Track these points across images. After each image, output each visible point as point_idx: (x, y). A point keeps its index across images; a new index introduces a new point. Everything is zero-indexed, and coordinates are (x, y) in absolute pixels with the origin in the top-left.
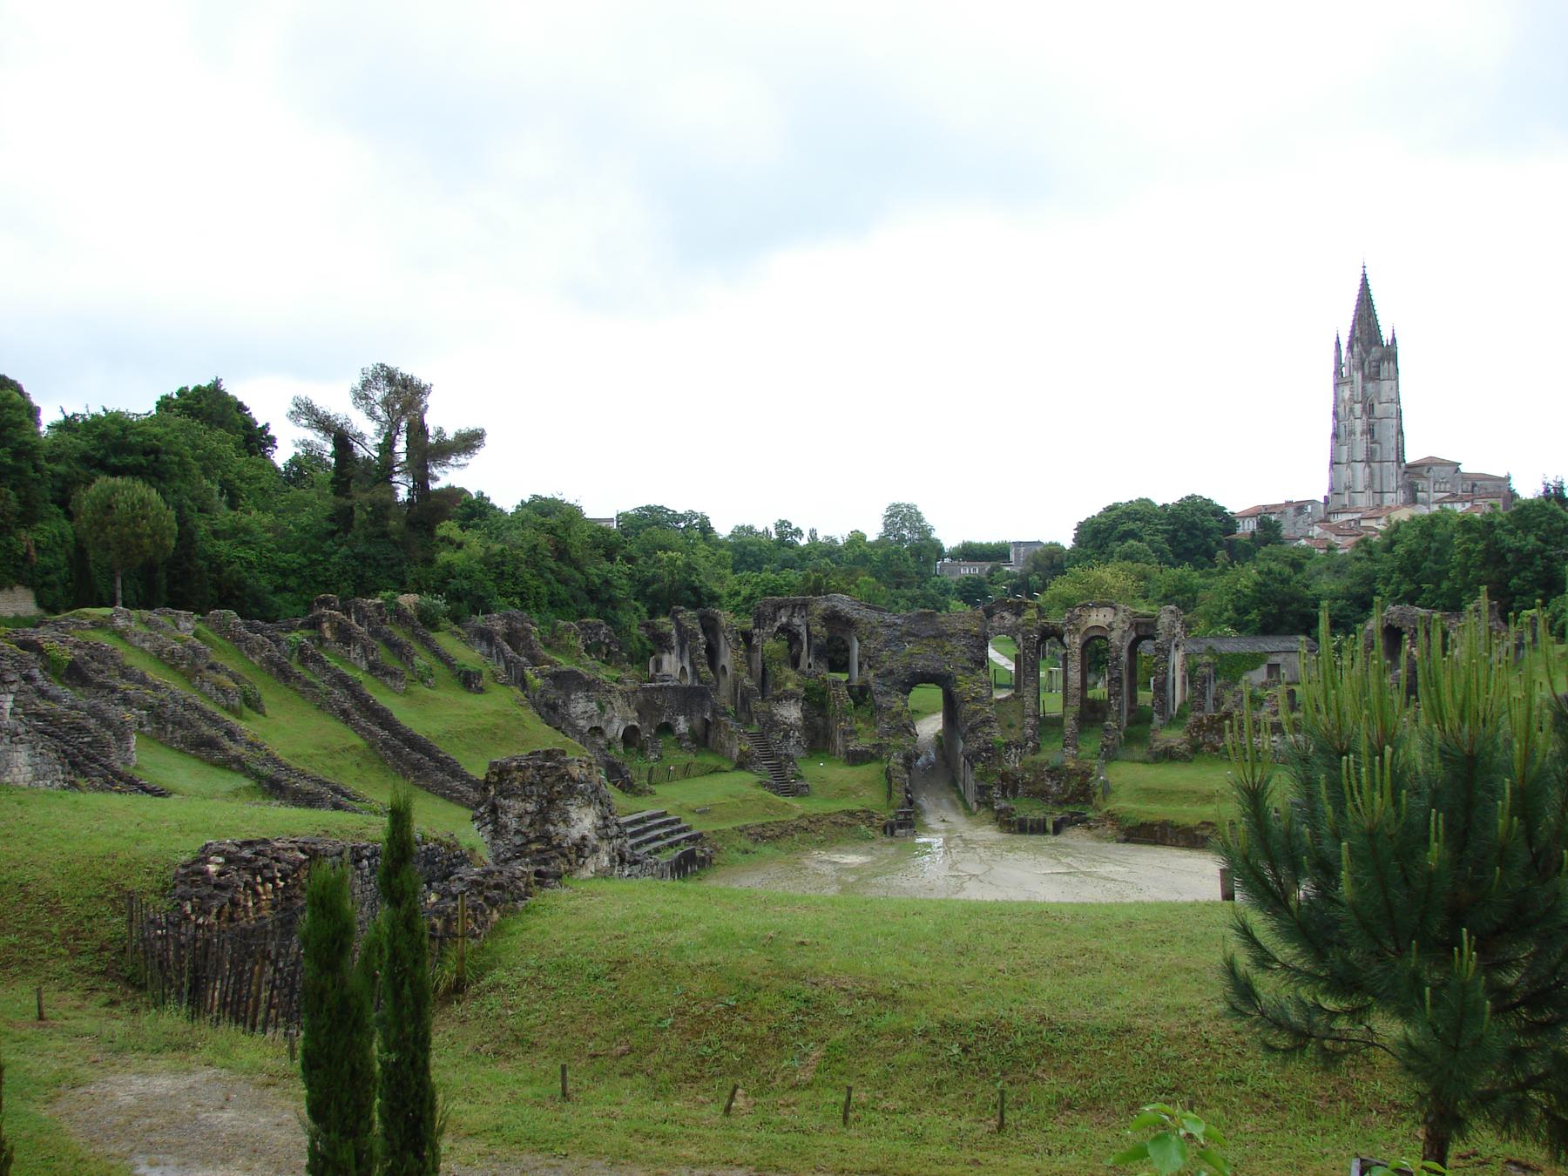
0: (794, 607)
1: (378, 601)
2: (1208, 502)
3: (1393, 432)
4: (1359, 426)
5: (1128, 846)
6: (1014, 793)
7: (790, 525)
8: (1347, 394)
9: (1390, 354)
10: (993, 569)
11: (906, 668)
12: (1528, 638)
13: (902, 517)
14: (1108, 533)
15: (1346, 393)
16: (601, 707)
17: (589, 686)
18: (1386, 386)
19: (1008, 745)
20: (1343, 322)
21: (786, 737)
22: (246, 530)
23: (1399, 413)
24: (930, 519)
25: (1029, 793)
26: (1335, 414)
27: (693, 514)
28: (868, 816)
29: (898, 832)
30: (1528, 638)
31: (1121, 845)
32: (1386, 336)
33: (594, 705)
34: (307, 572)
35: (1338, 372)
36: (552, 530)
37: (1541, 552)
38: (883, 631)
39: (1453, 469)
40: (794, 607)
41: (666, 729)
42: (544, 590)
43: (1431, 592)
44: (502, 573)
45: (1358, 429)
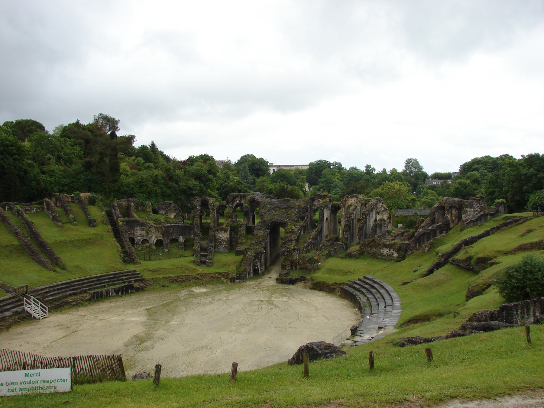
0: (241, 197)
1: (73, 195)
5: (313, 291)
6: (296, 268)
7: (370, 166)
10: (444, 182)
11: (270, 220)
13: (412, 164)
16: (147, 232)
17: (142, 225)
19: (294, 250)
21: (220, 244)
22: (53, 171)
24: (421, 164)
25: (301, 268)
28: (227, 275)
29: (236, 281)
31: (310, 290)
33: (144, 232)
34: (71, 185)
36: (168, 170)
37: (536, 175)
38: (268, 206)
40: (241, 197)
41: (176, 240)
42: (159, 191)
43: (499, 191)
44: (142, 185)
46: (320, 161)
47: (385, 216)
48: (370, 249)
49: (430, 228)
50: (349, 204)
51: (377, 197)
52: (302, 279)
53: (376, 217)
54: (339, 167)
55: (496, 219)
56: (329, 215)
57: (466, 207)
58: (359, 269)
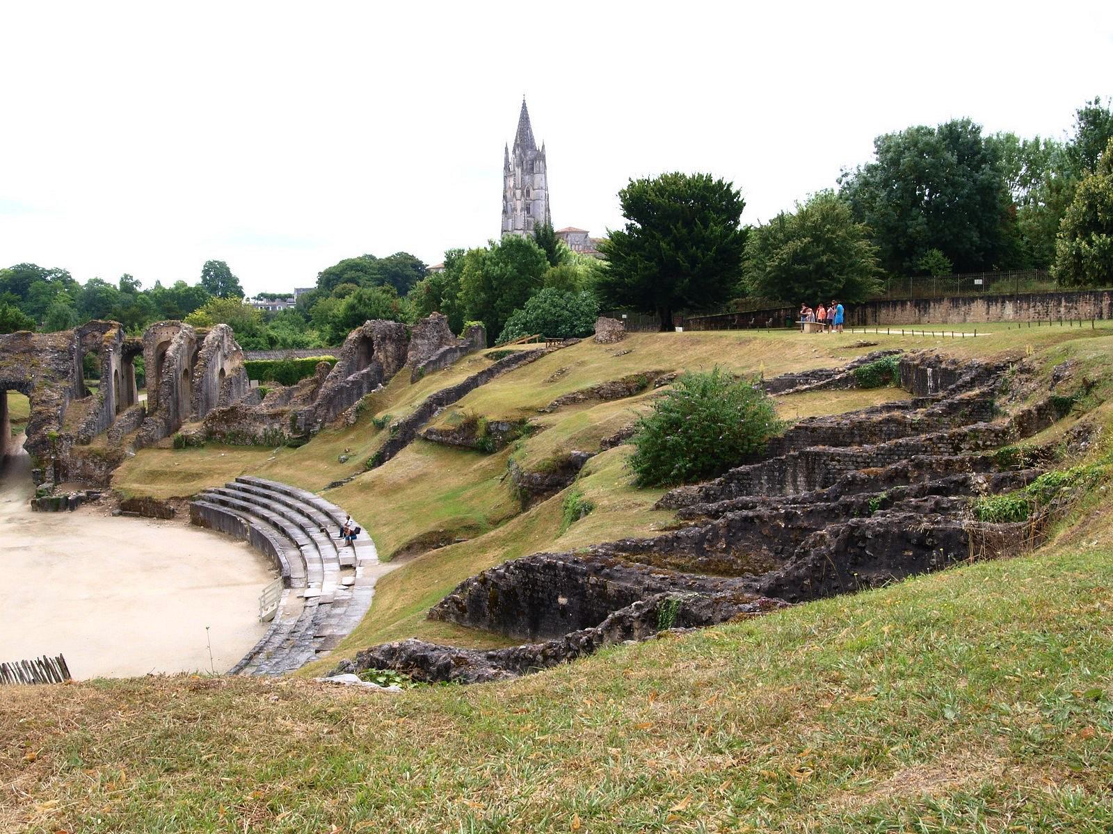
2: (412, 258)
3: (543, 209)
4: (519, 205)
8: (512, 184)
9: (541, 156)
12: (1016, 367)
14: (330, 279)
15: (511, 183)
18: (538, 177)
20: (510, 135)
23: (547, 197)
26: (505, 197)
27: (57, 270)
30: (1016, 367)
32: (538, 145)
35: (507, 168)
39: (584, 235)
45: (519, 208)
46: (23, 266)
47: (56, 396)
48: (227, 431)
49: (350, 378)
50: (163, 340)
51: (223, 325)
52: (91, 499)
53: (222, 364)
54: (66, 280)
55: (472, 357)
56: (119, 364)
57: (415, 338)
58: (220, 470)
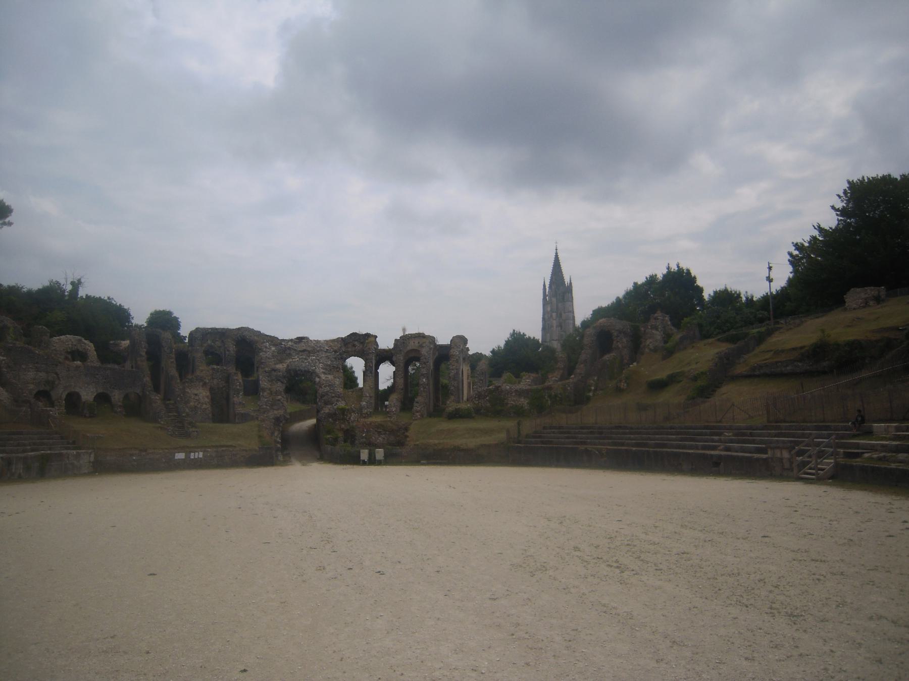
8: (549, 309)
